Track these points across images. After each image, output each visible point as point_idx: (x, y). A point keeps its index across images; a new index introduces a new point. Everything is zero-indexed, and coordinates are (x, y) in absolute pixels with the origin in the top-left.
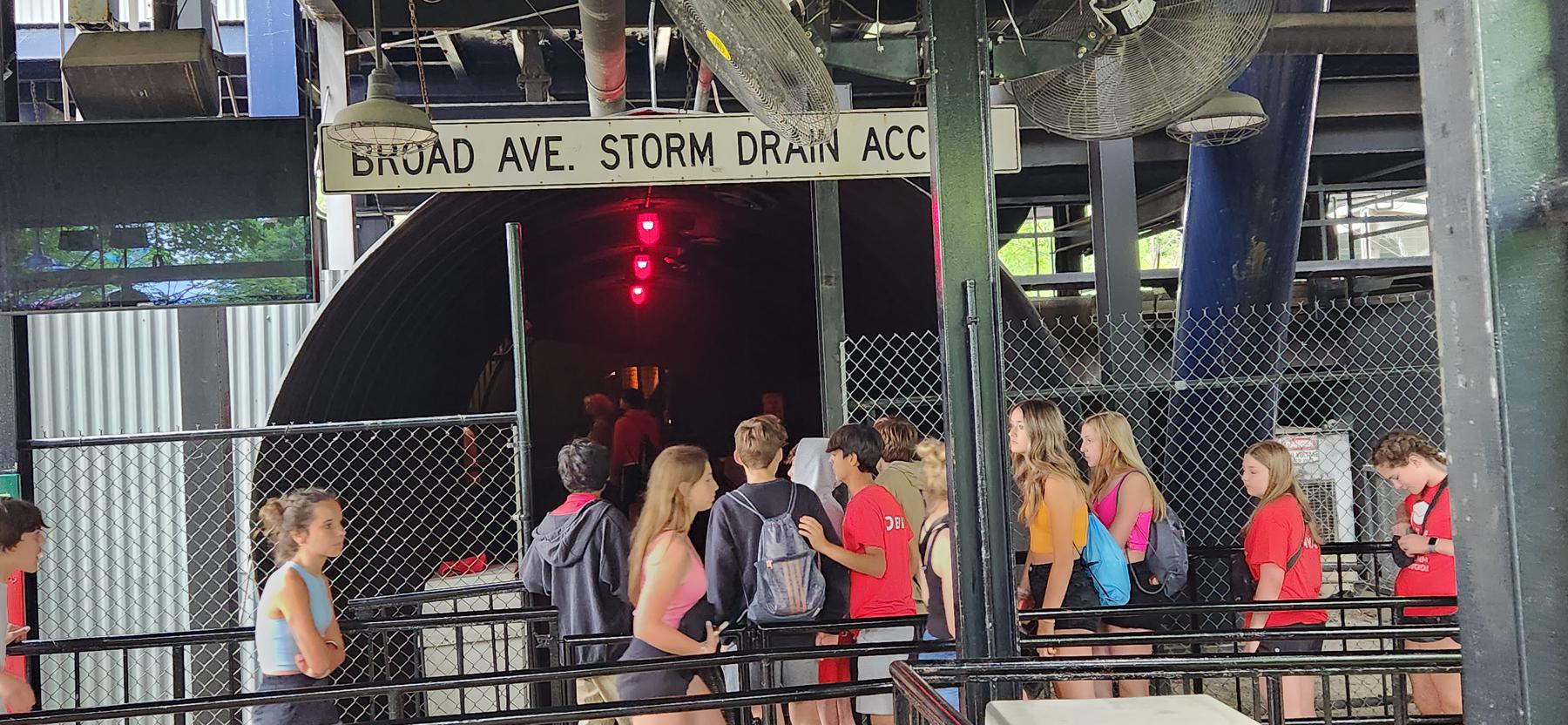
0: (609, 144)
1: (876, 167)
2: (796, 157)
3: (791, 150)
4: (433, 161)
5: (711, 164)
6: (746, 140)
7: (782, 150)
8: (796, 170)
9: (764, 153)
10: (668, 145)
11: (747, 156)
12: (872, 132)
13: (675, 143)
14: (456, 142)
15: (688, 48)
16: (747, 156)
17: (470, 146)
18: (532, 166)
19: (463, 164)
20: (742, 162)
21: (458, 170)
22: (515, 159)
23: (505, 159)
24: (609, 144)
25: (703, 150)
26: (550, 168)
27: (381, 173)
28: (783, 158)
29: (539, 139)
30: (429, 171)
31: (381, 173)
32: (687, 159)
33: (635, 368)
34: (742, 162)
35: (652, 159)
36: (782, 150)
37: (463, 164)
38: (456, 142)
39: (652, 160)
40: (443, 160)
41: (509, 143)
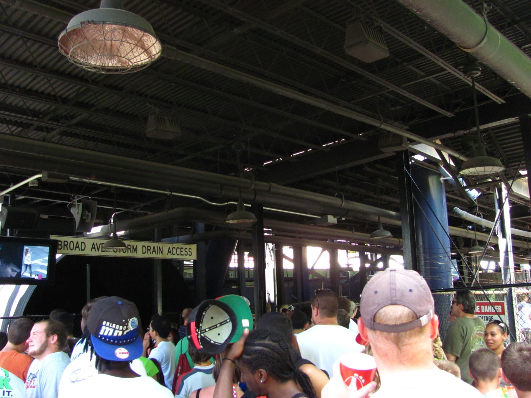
0: (190, 254)
1: (170, 256)
2: (154, 253)
3: (153, 251)
4: (76, 247)
5: (137, 253)
6: (144, 248)
7: (151, 251)
8: (154, 256)
9: (128, 250)
10: (64, 244)
11: (144, 252)
12: (169, 248)
13: (66, 243)
14: (82, 243)
15: (145, 213)
16: (144, 252)
17: (85, 246)
18: (98, 250)
19: (83, 248)
20: (143, 253)
21: (82, 250)
22: (94, 248)
23: (92, 248)
24: (190, 254)
25: (135, 249)
26: (102, 251)
27: (64, 249)
28: (151, 253)
29: (100, 243)
30: (75, 250)
31: (64, 249)
32: (132, 252)
33: (37, 186)
34: (143, 253)
35: (72, 244)
36: (151, 251)
37: (83, 248)
38: (82, 243)
39: (83, 244)
40: (78, 247)
41: (93, 244)
